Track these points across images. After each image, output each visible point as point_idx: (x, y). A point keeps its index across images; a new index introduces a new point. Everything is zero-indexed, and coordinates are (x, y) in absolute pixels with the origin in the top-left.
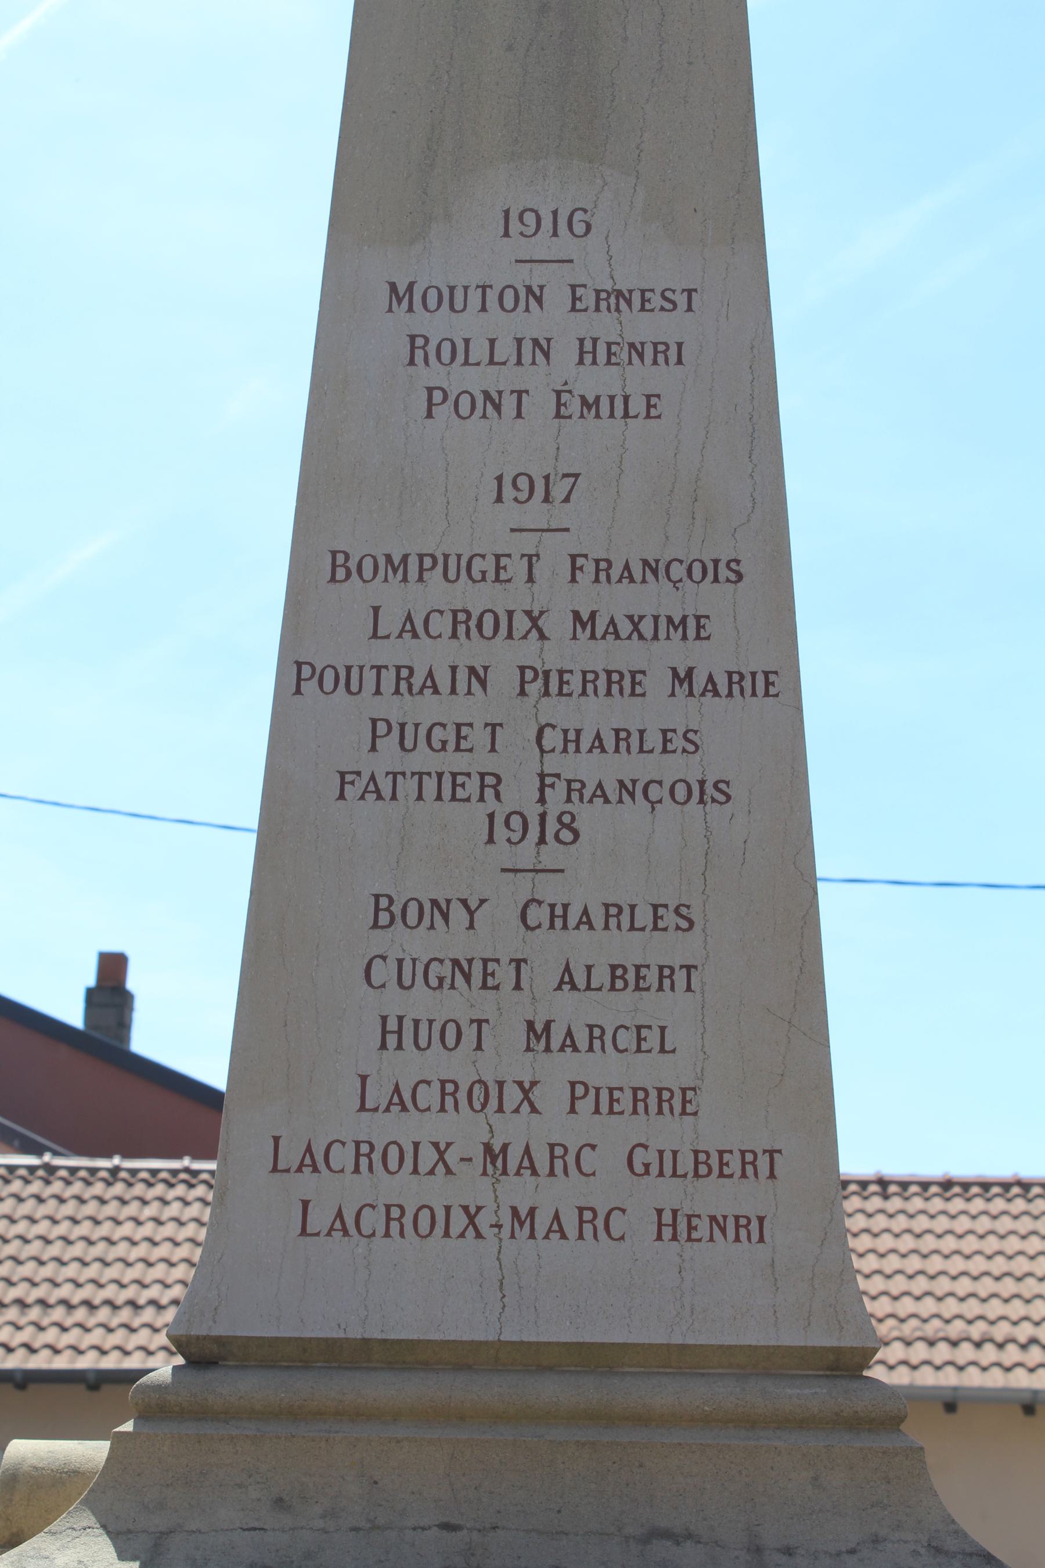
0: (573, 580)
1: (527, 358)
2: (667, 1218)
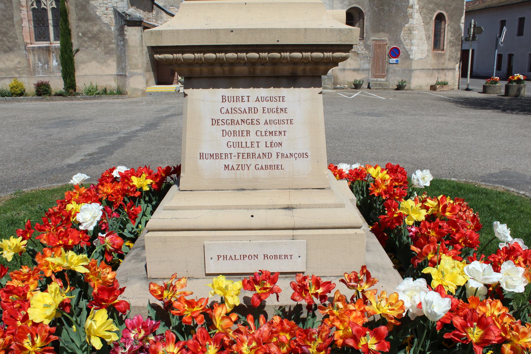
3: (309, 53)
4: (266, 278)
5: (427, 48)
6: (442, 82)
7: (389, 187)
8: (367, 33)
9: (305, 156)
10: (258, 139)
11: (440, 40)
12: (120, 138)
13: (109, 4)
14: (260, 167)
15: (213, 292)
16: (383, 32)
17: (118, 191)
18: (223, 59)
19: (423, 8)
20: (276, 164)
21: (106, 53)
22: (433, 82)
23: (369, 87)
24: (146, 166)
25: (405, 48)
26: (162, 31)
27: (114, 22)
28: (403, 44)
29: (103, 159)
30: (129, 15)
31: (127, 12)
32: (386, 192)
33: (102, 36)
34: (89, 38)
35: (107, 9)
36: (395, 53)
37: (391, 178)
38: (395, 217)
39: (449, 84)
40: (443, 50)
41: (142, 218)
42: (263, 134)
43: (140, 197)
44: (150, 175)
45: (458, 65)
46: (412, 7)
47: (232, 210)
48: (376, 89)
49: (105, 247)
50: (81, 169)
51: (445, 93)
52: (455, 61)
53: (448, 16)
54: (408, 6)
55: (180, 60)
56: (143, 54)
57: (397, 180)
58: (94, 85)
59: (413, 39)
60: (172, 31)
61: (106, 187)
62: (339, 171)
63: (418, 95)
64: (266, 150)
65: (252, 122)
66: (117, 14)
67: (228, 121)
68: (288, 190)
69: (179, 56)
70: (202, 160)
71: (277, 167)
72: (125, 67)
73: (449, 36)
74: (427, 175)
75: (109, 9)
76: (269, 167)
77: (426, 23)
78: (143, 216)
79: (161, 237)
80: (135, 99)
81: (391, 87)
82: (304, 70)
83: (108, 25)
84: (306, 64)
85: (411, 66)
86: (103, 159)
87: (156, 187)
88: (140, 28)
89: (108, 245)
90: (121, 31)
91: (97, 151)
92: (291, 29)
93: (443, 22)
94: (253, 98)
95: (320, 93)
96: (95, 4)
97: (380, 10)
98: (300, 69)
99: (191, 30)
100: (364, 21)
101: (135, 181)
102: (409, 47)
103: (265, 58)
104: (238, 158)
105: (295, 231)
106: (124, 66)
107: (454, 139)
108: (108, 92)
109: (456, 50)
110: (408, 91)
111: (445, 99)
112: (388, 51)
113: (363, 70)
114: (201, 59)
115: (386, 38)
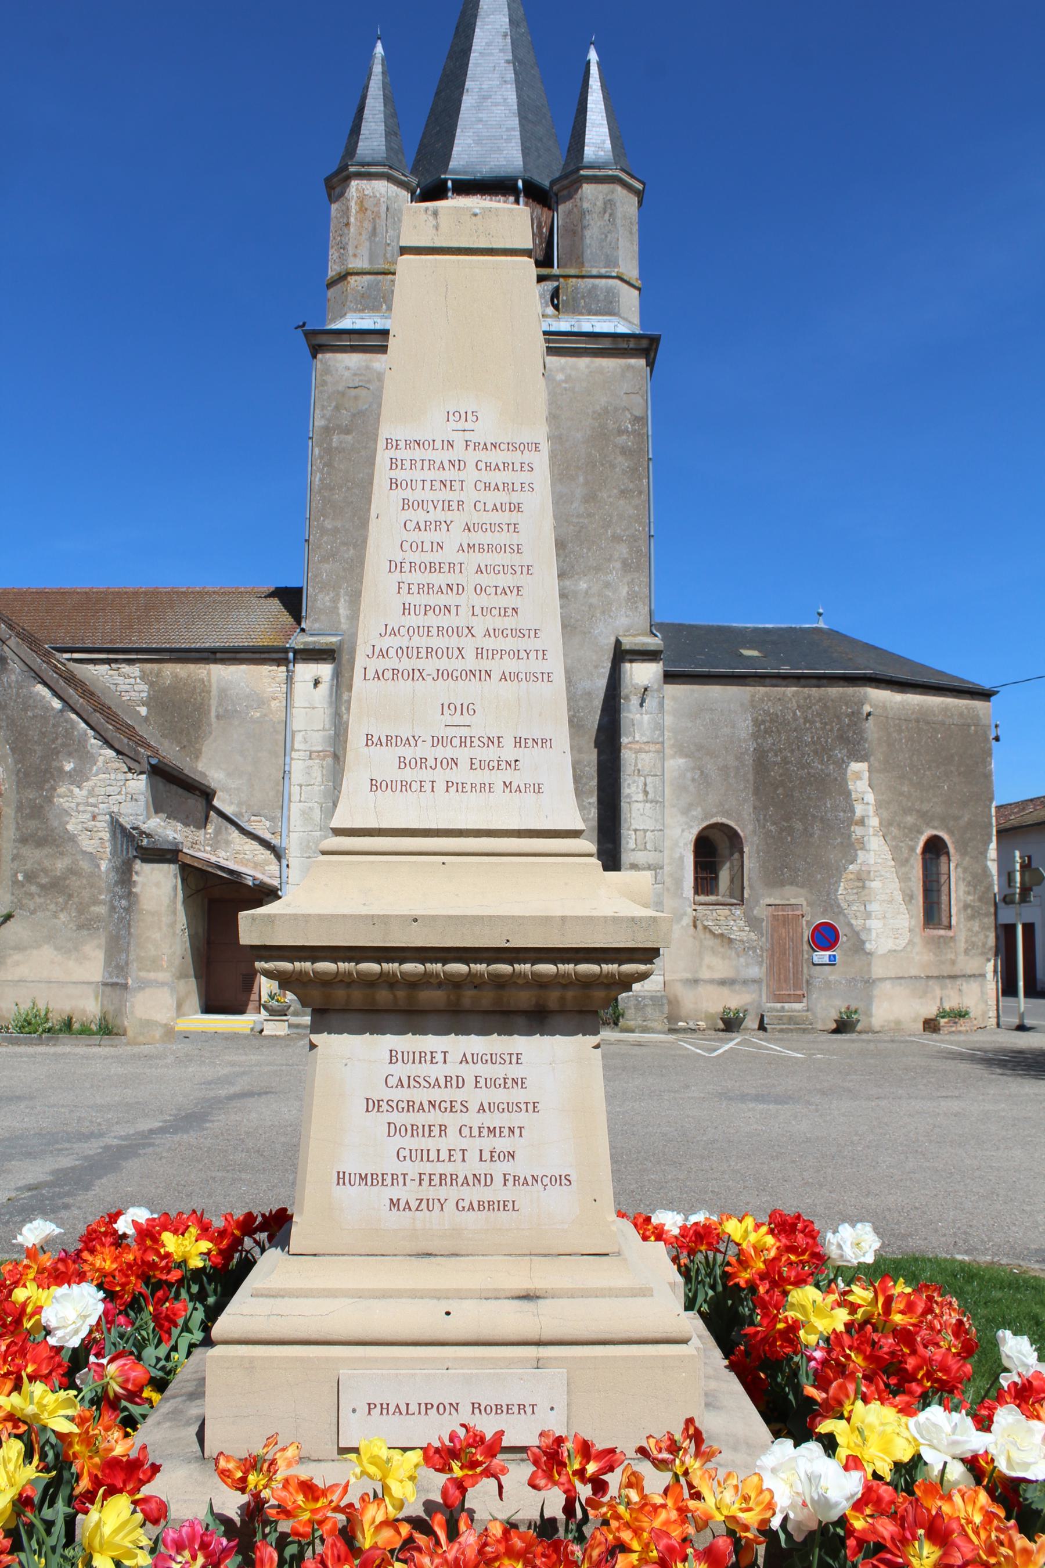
3: (572, 966)
4: (474, 1440)
5: (907, 925)
6: (952, 1010)
7: (771, 1263)
8: (751, 887)
9: (564, 1181)
10: (464, 1143)
11: (939, 903)
12: (107, 1148)
13: (101, 805)
14: (467, 1204)
15: (358, 1470)
16: (791, 884)
17: (130, 1266)
18: (394, 975)
19: (890, 824)
20: (502, 1198)
21: (80, 927)
22: (930, 1010)
23: (762, 1027)
24: (194, 1212)
25: (851, 925)
26: (275, 915)
27: (108, 850)
28: (845, 915)
29: (66, 1200)
30: (149, 836)
31: (144, 827)
32: (763, 1276)
33: (74, 882)
34: (43, 887)
35: (94, 818)
36: (826, 937)
37: (778, 1244)
38: (779, 1330)
39: (972, 1015)
40: (949, 927)
41: (179, 1336)
42: (475, 1132)
43: (180, 1282)
44: (205, 1230)
45: (990, 966)
46: (862, 822)
47: (404, 1300)
48: (781, 1031)
49: (105, 1388)
50: (8, 1222)
51: (962, 1038)
52: (983, 954)
53: (956, 843)
54: (851, 821)
55: (307, 973)
56: (174, 934)
57: (791, 1249)
58: (42, 1006)
59: (870, 902)
60: (295, 917)
61: (100, 1256)
62: (655, 1228)
63: (889, 1046)
64: (481, 1169)
65: (452, 1107)
66: (118, 831)
67: (401, 1105)
68: (528, 1258)
69: (307, 966)
70: (341, 1186)
71: (505, 1206)
72: (127, 964)
73: (961, 893)
74: (866, 1237)
75: (99, 818)
76: (486, 1205)
77: (901, 862)
78: (182, 1331)
79: (242, 1358)
80: (145, 1049)
81: (820, 1026)
82: (562, 999)
83: (92, 857)
84: (565, 986)
85: (869, 971)
86: (66, 1200)
87: (219, 1260)
88: (172, 866)
89: (112, 1382)
90: (123, 873)
91: (49, 1178)
92: (534, 918)
93: (943, 859)
94: (454, 1057)
95: (597, 1047)
96: (66, 805)
97: (782, 830)
98: (553, 998)
99: (332, 916)
100: (742, 857)
101: (170, 1242)
102: (860, 922)
103: (482, 975)
104: (420, 1184)
105: (541, 1349)
106: (122, 963)
107: (976, 1157)
108: (76, 1026)
109: (983, 928)
110: (864, 1036)
111: (961, 1054)
112: (807, 933)
113: (745, 982)
114: (350, 974)
115: (801, 901)
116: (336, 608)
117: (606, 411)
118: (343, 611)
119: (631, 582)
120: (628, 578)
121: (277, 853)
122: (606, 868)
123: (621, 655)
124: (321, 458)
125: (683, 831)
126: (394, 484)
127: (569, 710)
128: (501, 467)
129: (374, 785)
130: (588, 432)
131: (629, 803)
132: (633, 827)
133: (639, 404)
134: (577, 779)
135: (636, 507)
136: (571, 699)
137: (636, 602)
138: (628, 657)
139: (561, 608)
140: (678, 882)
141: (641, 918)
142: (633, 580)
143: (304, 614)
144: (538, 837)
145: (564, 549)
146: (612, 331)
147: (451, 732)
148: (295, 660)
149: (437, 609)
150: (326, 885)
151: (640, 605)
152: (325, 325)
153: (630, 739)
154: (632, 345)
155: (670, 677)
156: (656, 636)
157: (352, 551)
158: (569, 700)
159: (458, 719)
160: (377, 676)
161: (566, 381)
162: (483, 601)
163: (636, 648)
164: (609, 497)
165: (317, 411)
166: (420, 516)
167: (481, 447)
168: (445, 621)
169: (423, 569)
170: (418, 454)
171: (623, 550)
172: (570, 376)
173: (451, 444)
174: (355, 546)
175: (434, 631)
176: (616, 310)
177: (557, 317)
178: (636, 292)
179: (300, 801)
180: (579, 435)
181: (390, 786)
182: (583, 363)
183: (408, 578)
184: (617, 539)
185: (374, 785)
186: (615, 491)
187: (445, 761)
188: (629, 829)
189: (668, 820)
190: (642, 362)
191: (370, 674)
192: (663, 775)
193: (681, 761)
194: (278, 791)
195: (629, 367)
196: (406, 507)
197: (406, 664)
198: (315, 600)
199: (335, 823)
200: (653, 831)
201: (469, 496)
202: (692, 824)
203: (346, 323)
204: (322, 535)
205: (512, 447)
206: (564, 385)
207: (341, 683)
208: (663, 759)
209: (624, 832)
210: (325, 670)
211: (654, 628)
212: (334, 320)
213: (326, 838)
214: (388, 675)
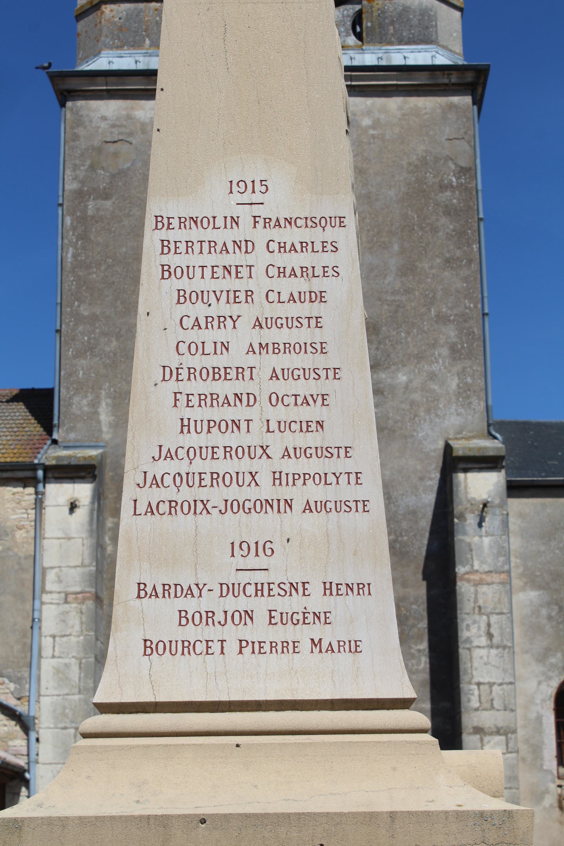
0: (255, 227)
1: (229, 225)
2: (328, 586)
26: (23, 820)
60: (49, 821)
99: (97, 818)
116: (96, 413)
117: (424, 161)
118: (105, 416)
119: (462, 374)
120: (458, 367)
121: (25, 723)
122: (445, 746)
123: (453, 464)
124: (74, 228)
125: (539, 683)
126: (166, 271)
127: (389, 534)
128: (298, 247)
129: (149, 647)
130: (403, 189)
131: (469, 649)
132: (476, 680)
133: (464, 152)
134: (402, 620)
135: (465, 279)
136: (392, 519)
137: (468, 397)
138: (462, 465)
139: (376, 406)
140: (536, 750)
141: (492, 813)
142: (464, 369)
143: (56, 421)
144: (357, 709)
145: (377, 335)
146: (429, 62)
147: (244, 578)
148: (46, 480)
149: (223, 424)
150: (88, 777)
151: (474, 400)
152: (75, 66)
153: (468, 568)
154: (454, 80)
155: (514, 489)
156: (495, 438)
157: (114, 343)
158: (389, 521)
159: (252, 562)
160: (150, 510)
161: (373, 127)
162: (280, 413)
163: (471, 454)
164: (431, 267)
165: (68, 172)
166: (200, 311)
167: (272, 224)
168: (233, 439)
169: (204, 376)
170: (195, 234)
171: (451, 333)
172: (378, 119)
173: (235, 221)
174: (118, 336)
175: (220, 453)
176: (434, 38)
177: (360, 48)
178: (458, 14)
179: (53, 657)
180: (392, 193)
181: (169, 647)
182: (394, 103)
183: (187, 387)
184: (442, 319)
185: (149, 647)
186: (438, 260)
187: (237, 615)
188: (470, 683)
189: (520, 670)
190: (468, 100)
191: (142, 508)
192: (511, 612)
193: (533, 595)
194: (25, 644)
195: (452, 106)
196: (182, 300)
197: (186, 494)
198: (72, 404)
199: (99, 698)
200: (501, 684)
201: (259, 284)
202: (550, 674)
203: (101, 63)
204: (76, 325)
205: (312, 222)
206: (371, 132)
207: (106, 507)
208: (510, 593)
209: (464, 686)
210: (83, 491)
211: (493, 427)
212: (86, 59)
213: (88, 716)
214: (164, 508)
